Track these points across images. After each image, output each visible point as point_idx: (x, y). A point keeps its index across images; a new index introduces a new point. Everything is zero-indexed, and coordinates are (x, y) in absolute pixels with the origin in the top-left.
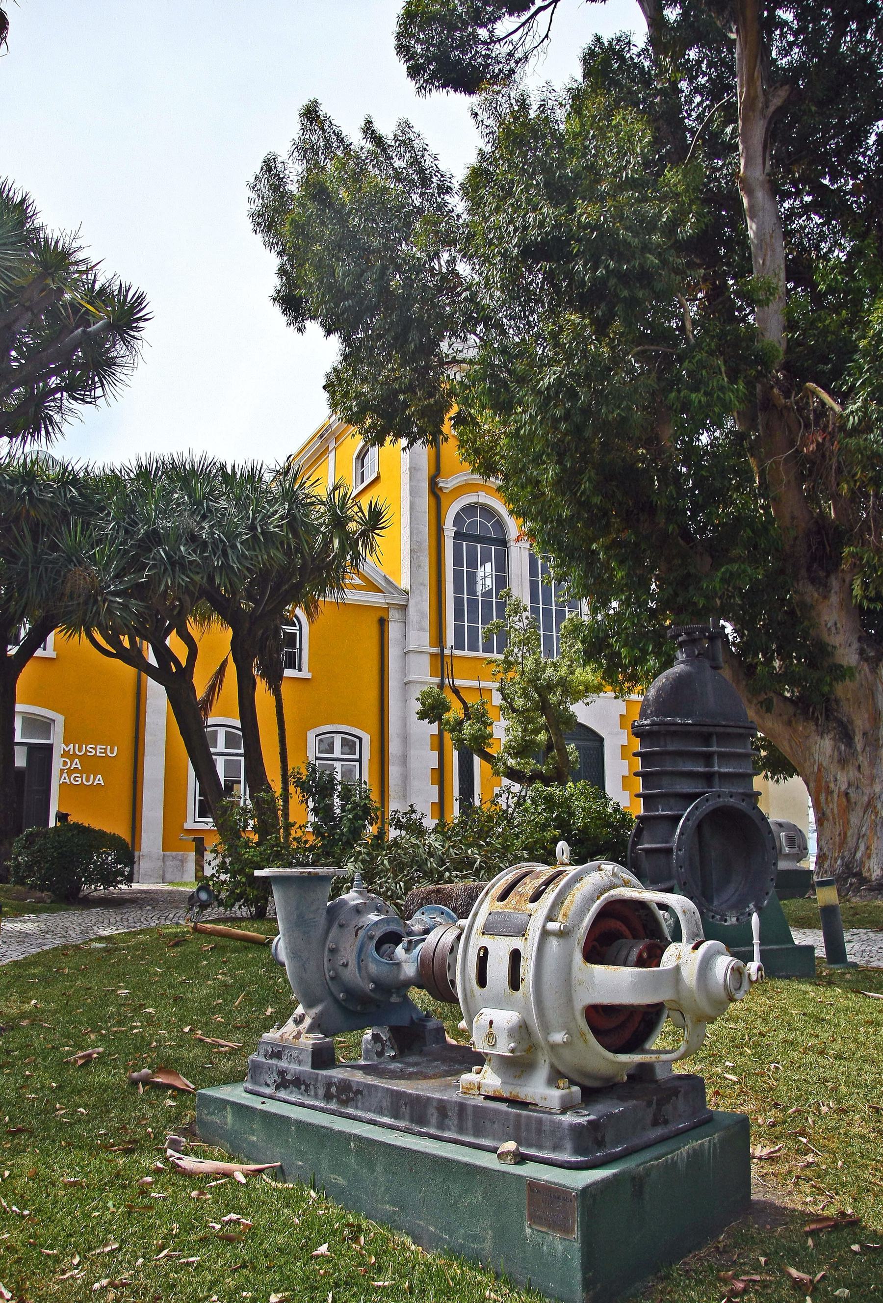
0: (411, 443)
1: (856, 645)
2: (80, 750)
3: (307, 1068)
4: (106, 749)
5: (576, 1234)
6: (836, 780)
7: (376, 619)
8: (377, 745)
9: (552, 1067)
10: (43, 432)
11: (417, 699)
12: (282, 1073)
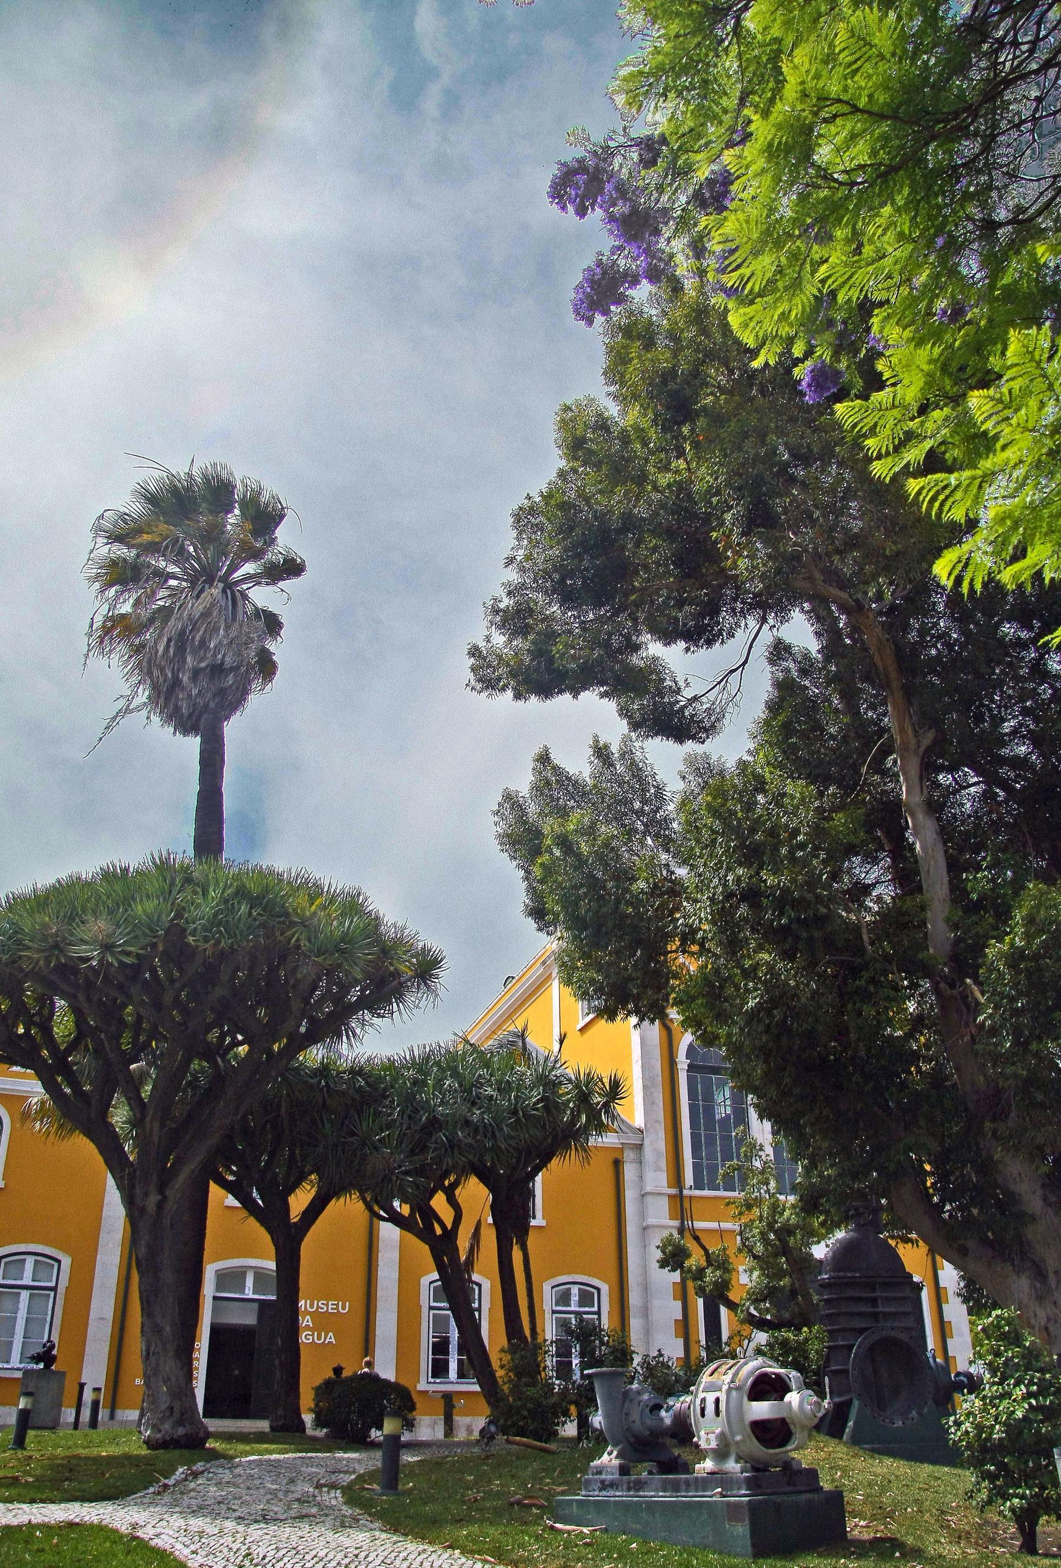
0: (642, 1020)
1: (1039, 1192)
2: (312, 1306)
3: (617, 1476)
4: (337, 1305)
5: (747, 1522)
6: (1036, 1316)
7: (611, 1160)
8: (616, 1296)
9: (737, 1454)
10: (344, 1038)
11: (658, 1247)
12: (603, 1482)
